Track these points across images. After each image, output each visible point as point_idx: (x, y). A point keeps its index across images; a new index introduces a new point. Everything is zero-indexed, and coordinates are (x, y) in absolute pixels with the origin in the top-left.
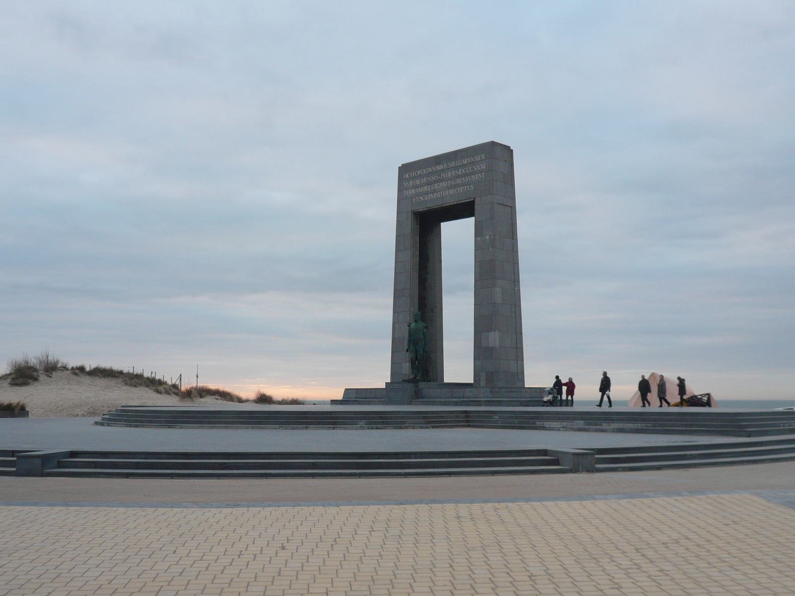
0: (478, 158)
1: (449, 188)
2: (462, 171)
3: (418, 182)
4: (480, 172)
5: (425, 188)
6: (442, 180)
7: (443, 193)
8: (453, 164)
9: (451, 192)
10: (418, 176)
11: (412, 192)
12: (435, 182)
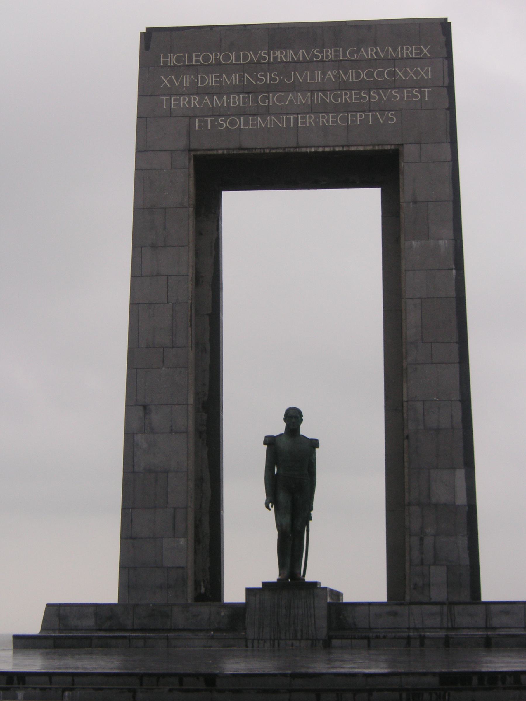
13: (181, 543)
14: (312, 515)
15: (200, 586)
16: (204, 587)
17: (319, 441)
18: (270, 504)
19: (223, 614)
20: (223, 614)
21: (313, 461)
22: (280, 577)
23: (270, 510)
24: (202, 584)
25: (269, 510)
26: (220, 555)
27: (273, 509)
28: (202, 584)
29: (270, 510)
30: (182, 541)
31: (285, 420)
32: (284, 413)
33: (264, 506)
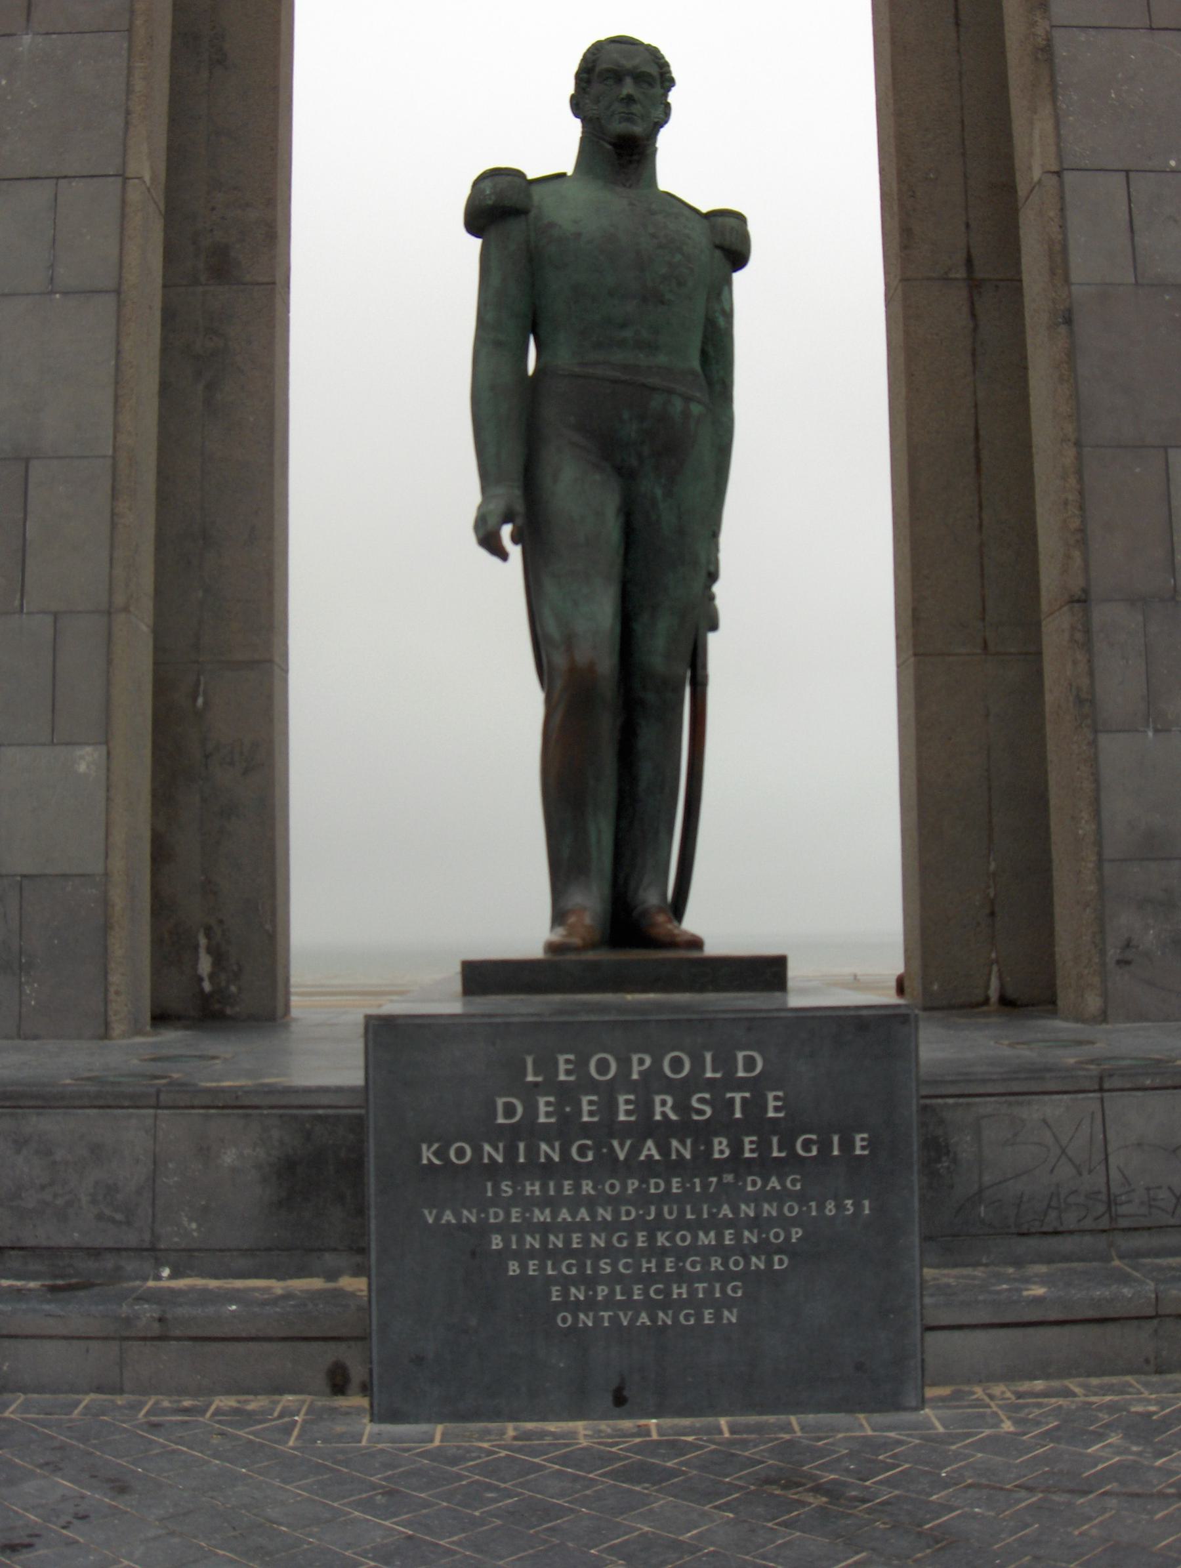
13: (82, 768)
14: (720, 602)
15: (196, 948)
16: (209, 951)
17: (752, 228)
18: (506, 531)
19: (229, 1157)
20: (229, 1157)
21: (721, 321)
22: (561, 931)
23: (503, 555)
24: (203, 941)
25: (495, 561)
26: (273, 828)
27: (515, 552)
28: (203, 941)
29: (503, 555)
30: (86, 760)
31: (577, 105)
32: (574, 65)
33: (471, 538)
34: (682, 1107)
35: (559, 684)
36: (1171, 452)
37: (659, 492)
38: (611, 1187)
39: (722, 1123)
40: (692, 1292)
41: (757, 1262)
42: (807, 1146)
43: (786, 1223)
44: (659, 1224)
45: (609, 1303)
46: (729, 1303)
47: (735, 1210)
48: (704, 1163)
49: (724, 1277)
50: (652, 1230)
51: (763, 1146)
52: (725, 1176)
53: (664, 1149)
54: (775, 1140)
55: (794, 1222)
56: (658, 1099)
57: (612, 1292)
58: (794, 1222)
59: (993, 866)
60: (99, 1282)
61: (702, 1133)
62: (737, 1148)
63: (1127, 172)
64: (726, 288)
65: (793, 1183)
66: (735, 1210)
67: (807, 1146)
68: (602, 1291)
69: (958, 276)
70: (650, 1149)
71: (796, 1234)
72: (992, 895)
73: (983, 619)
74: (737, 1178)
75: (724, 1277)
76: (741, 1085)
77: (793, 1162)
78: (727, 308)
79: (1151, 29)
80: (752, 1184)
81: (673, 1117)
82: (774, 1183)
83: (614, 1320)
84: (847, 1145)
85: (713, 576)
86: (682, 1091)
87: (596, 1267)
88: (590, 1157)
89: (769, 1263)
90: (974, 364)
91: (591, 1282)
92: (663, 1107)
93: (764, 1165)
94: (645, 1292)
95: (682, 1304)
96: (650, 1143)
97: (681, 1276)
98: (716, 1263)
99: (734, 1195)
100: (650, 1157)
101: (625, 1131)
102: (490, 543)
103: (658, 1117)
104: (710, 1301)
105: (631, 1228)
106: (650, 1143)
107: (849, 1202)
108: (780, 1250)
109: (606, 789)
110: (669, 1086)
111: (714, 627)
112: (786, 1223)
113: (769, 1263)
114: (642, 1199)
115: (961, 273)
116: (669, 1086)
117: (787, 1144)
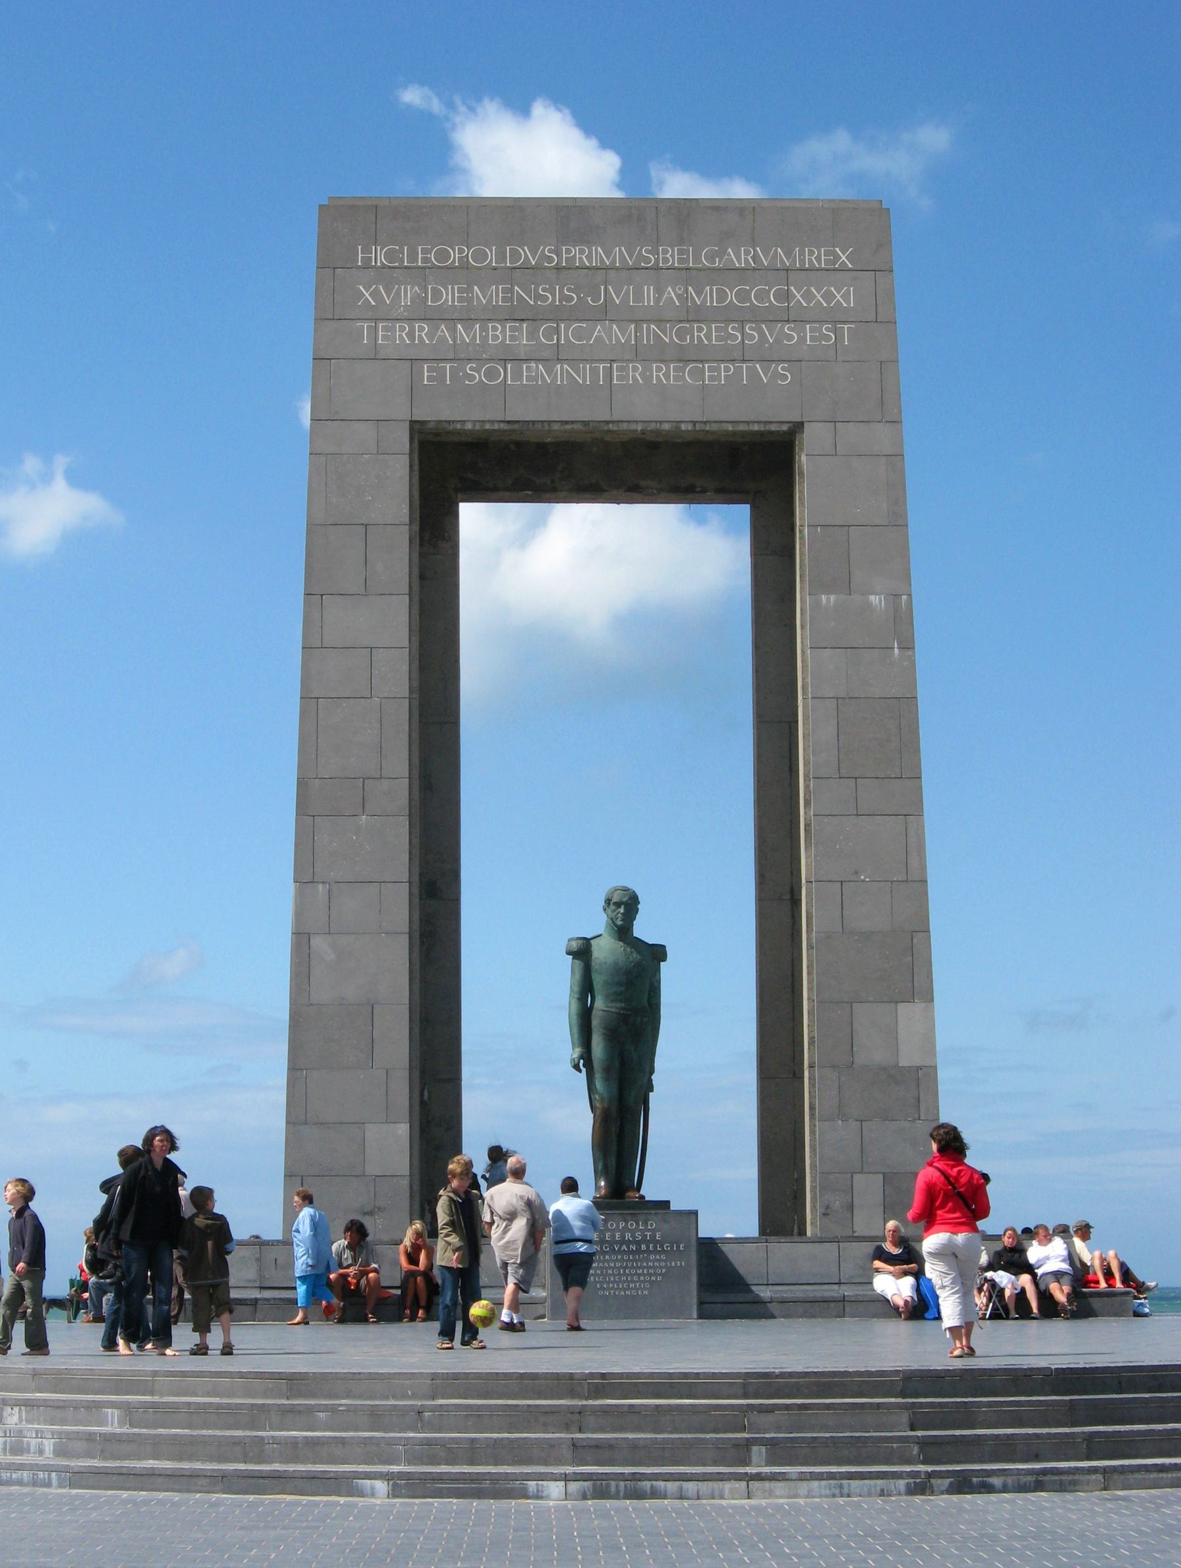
0: (815, 257)
1: (639, 354)
2: (722, 296)
3: (450, 296)
4: (835, 318)
5: (499, 334)
6: (604, 314)
7: (609, 373)
8: (671, 256)
9: (659, 373)
10: (451, 268)
11: (411, 335)
12: (560, 315)
21: (656, 984)
23: (580, 1071)
27: (584, 1070)
34: (633, 1236)
35: (598, 1112)
36: (854, 1005)
37: (632, 1049)
38: (614, 1257)
39: (644, 1240)
40: (635, 1286)
41: (653, 1278)
42: (667, 1247)
43: (661, 1268)
44: (627, 1267)
45: (613, 1288)
46: (645, 1288)
47: (647, 1264)
48: (639, 1251)
49: (645, 1281)
50: (625, 1268)
51: (655, 1247)
52: (763, 1449)
53: (628, 1248)
54: (658, 1246)
55: (663, 1267)
56: (627, 1234)
57: (614, 1285)
58: (663, 1267)
59: (796, 1176)
60: (199, 1495)
61: (638, 1243)
62: (648, 1247)
63: (842, 882)
64: (658, 973)
65: (663, 1257)
66: (647, 1264)
67: (667, 1247)
68: (611, 1285)
69: (786, 898)
70: (624, 1247)
71: (664, 1271)
72: (795, 1189)
73: (794, 1061)
74: (648, 1255)
75: (645, 1281)
76: (649, 1230)
77: (663, 1251)
78: (658, 979)
79: (857, 815)
80: (652, 1257)
81: (630, 1239)
82: (658, 1257)
83: (614, 1293)
84: (678, 1247)
85: (652, 1072)
86: (633, 1232)
87: (609, 1279)
88: (608, 1249)
89: (656, 1278)
90: (793, 941)
91: (605, 1276)
92: (628, 1236)
93: (655, 1252)
94: (623, 1285)
95: (632, 1289)
96: (624, 1246)
97: (632, 1281)
98: (642, 1278)
99: (647, 1260)
100: (624, 1250)
101: (617, 1242)
102: (576, 1067)
103: (627, 1239)
104: (640, 1288)
105: (619, 1268)
106: (624, 1246)
107: (678, 1263)
108: (659, 1275)
109: (614, 1147)
110: (630, 1231)
111: (652, 1091)
112: (661, 1268)
113: (656, 1278)
114: (622, 1260)
115: (787, 897)
116: (630, 1231)
117: (662, 1246)
